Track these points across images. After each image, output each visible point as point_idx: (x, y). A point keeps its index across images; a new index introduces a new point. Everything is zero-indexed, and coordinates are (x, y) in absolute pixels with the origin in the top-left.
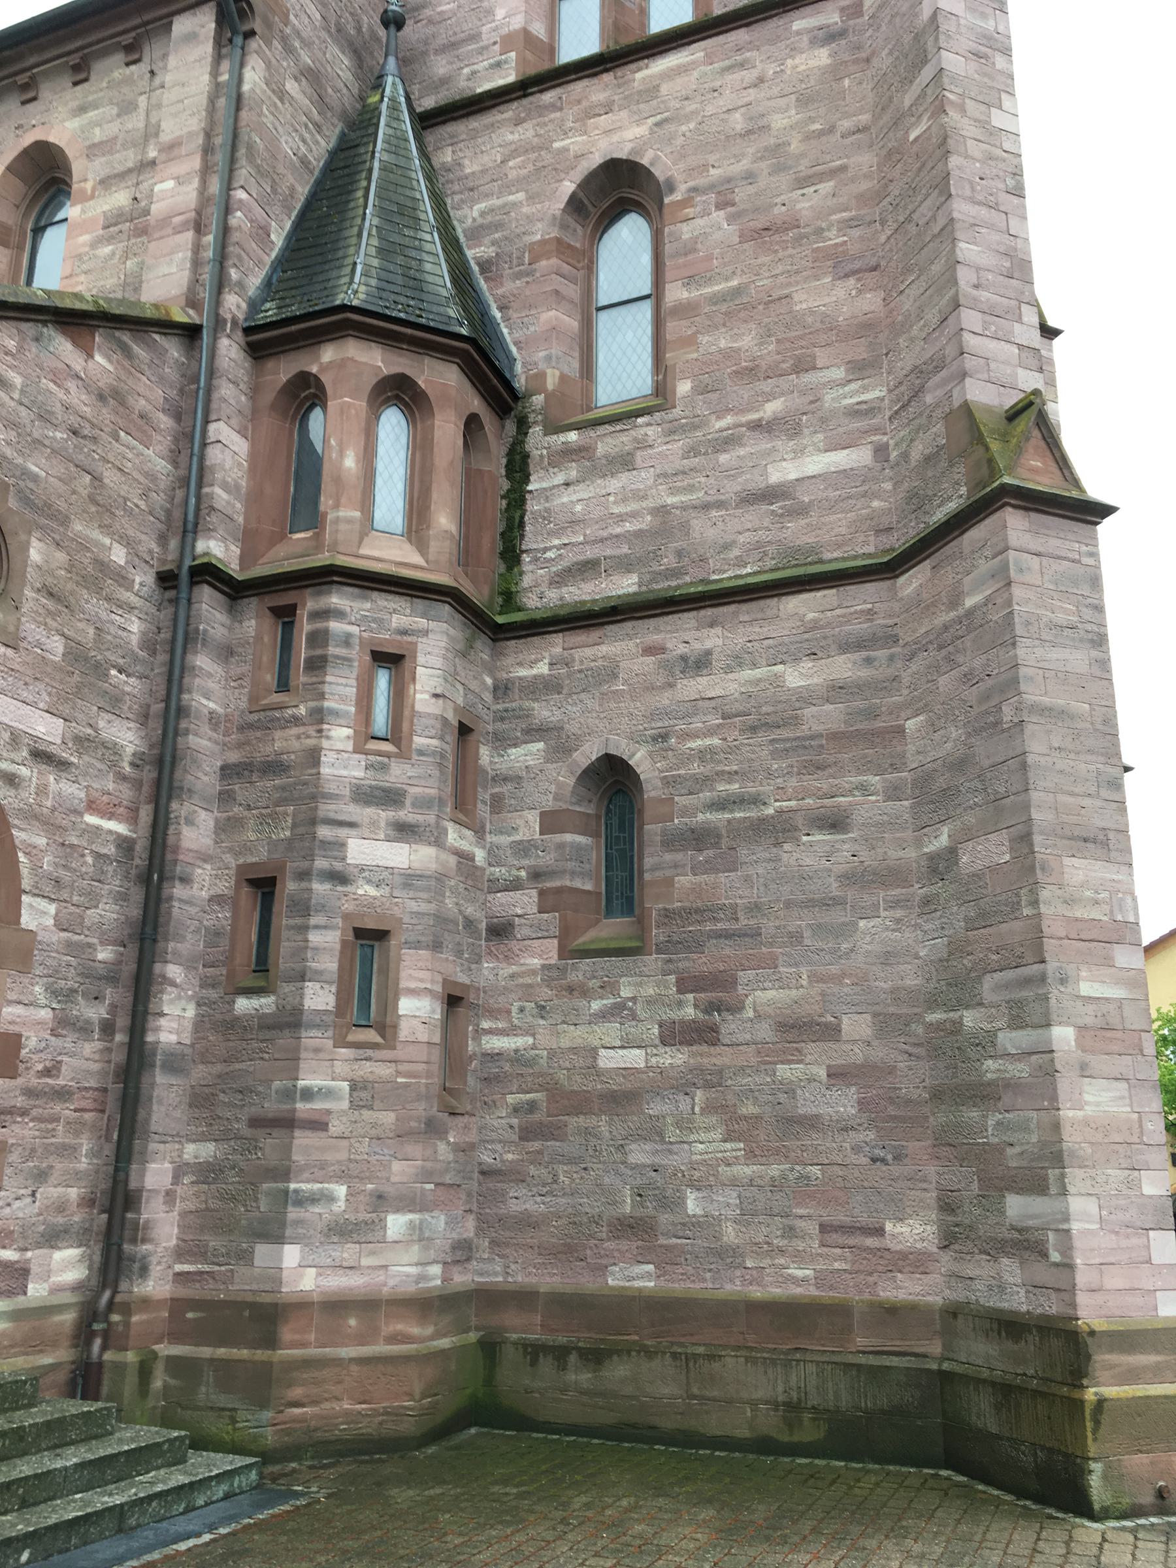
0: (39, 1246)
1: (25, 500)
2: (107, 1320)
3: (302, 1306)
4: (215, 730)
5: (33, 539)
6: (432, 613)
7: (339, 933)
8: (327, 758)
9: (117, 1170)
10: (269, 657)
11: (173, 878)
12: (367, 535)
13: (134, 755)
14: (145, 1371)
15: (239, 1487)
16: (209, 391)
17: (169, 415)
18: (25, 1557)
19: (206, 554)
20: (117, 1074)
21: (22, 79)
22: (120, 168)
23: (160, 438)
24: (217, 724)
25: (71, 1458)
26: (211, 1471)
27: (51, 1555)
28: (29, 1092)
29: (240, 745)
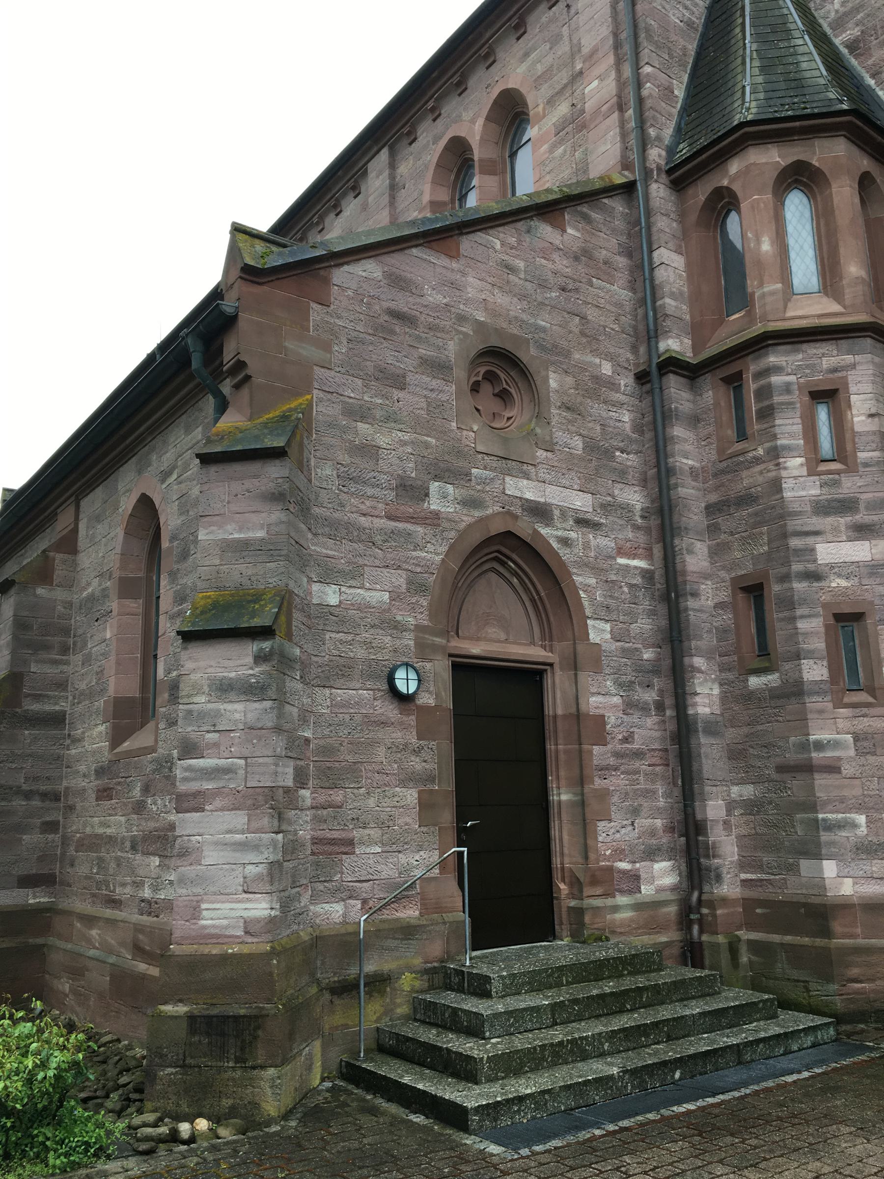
0: (642, 860)
1: (542, 348)
2: (699, 913)
3: (844, 907)
4: (695, 480)
5: (550, 373)
6: (857, 348)
7: (821, 619)
8: (787, 485)
9: (685, 806)
10: (728, 416)
11: (685, 595)
12: (789, 300)
13: (642, 509)
14: (733, 948)
15: (822, 1039)
16: (649, 227)
17: (624, 256)
18: (677, 1075)
19: (667, 351)
20: (672, 740)
21: (483, 52)
22: (558, 87)
23: (620, 275)
24: (697, 475)
25: (695, 1008)
26: (798, 1025)
27: (695, 1076)
28: (617, 755)
29: (717, 488)
